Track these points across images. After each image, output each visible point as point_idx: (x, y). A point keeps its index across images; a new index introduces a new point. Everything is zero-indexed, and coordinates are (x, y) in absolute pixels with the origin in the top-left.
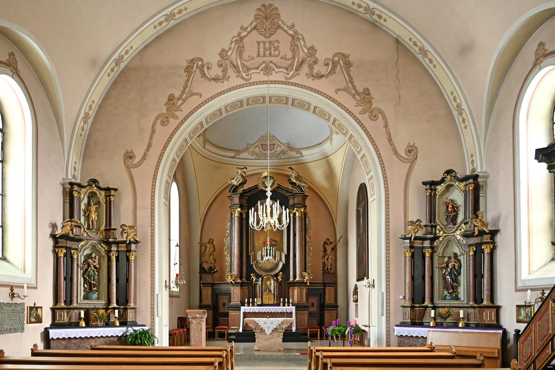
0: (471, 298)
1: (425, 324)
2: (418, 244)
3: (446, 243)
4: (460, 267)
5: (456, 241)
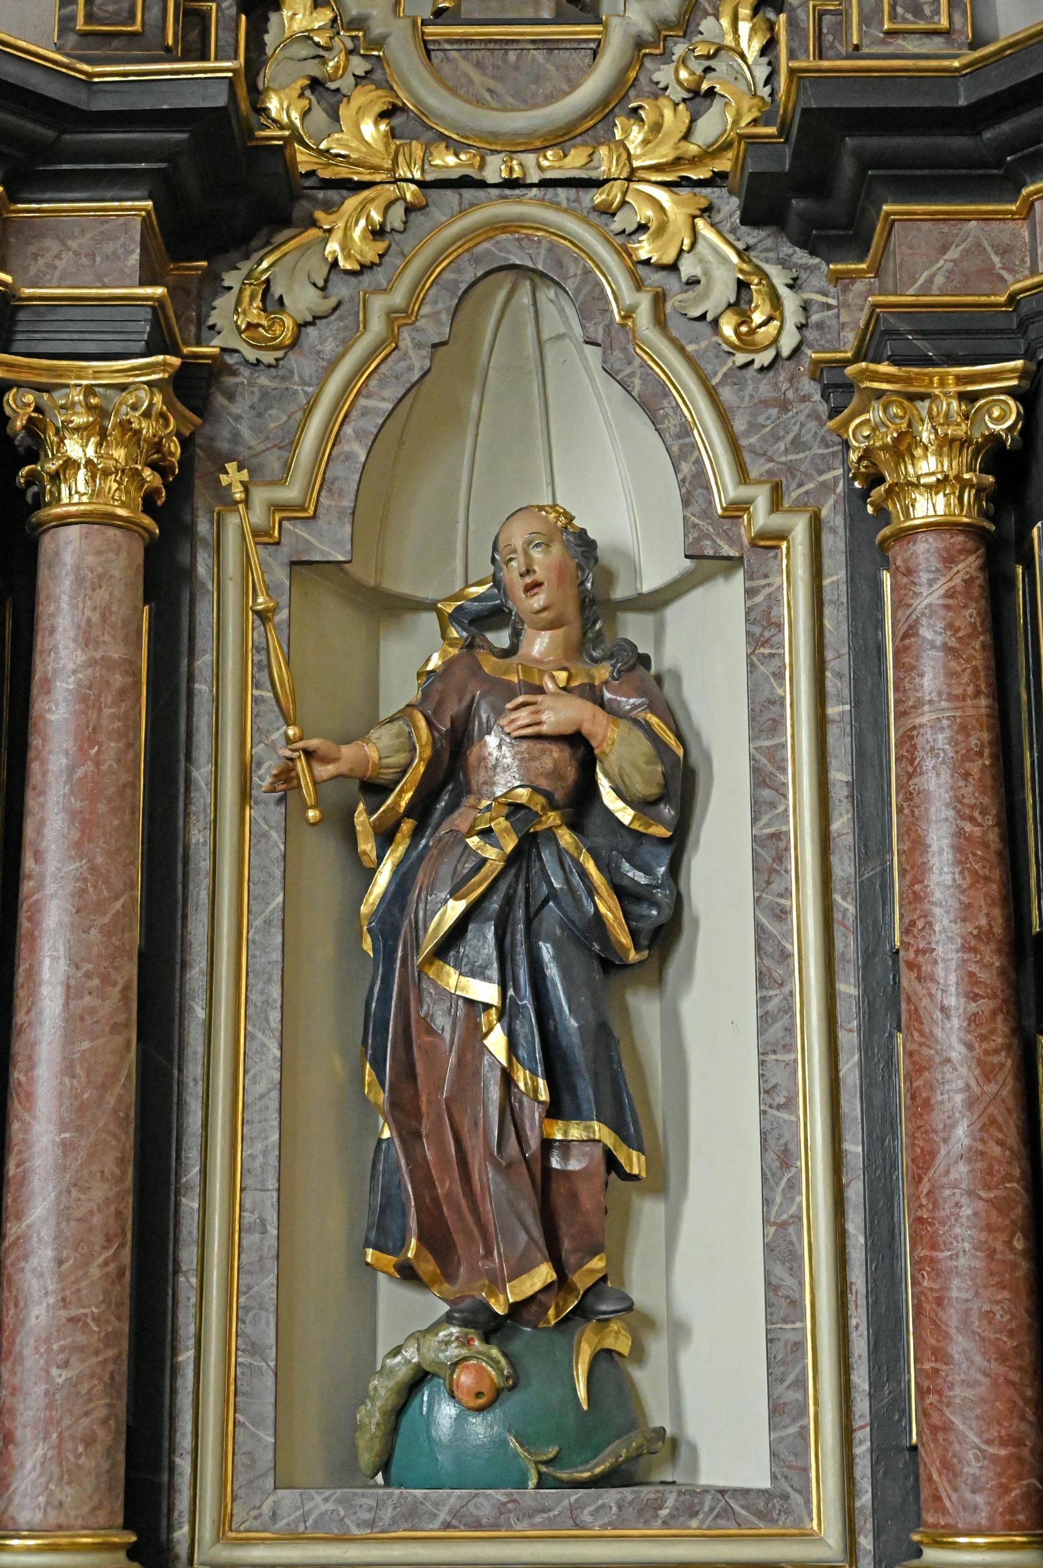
4: (679, 788)
5: (617, 286)
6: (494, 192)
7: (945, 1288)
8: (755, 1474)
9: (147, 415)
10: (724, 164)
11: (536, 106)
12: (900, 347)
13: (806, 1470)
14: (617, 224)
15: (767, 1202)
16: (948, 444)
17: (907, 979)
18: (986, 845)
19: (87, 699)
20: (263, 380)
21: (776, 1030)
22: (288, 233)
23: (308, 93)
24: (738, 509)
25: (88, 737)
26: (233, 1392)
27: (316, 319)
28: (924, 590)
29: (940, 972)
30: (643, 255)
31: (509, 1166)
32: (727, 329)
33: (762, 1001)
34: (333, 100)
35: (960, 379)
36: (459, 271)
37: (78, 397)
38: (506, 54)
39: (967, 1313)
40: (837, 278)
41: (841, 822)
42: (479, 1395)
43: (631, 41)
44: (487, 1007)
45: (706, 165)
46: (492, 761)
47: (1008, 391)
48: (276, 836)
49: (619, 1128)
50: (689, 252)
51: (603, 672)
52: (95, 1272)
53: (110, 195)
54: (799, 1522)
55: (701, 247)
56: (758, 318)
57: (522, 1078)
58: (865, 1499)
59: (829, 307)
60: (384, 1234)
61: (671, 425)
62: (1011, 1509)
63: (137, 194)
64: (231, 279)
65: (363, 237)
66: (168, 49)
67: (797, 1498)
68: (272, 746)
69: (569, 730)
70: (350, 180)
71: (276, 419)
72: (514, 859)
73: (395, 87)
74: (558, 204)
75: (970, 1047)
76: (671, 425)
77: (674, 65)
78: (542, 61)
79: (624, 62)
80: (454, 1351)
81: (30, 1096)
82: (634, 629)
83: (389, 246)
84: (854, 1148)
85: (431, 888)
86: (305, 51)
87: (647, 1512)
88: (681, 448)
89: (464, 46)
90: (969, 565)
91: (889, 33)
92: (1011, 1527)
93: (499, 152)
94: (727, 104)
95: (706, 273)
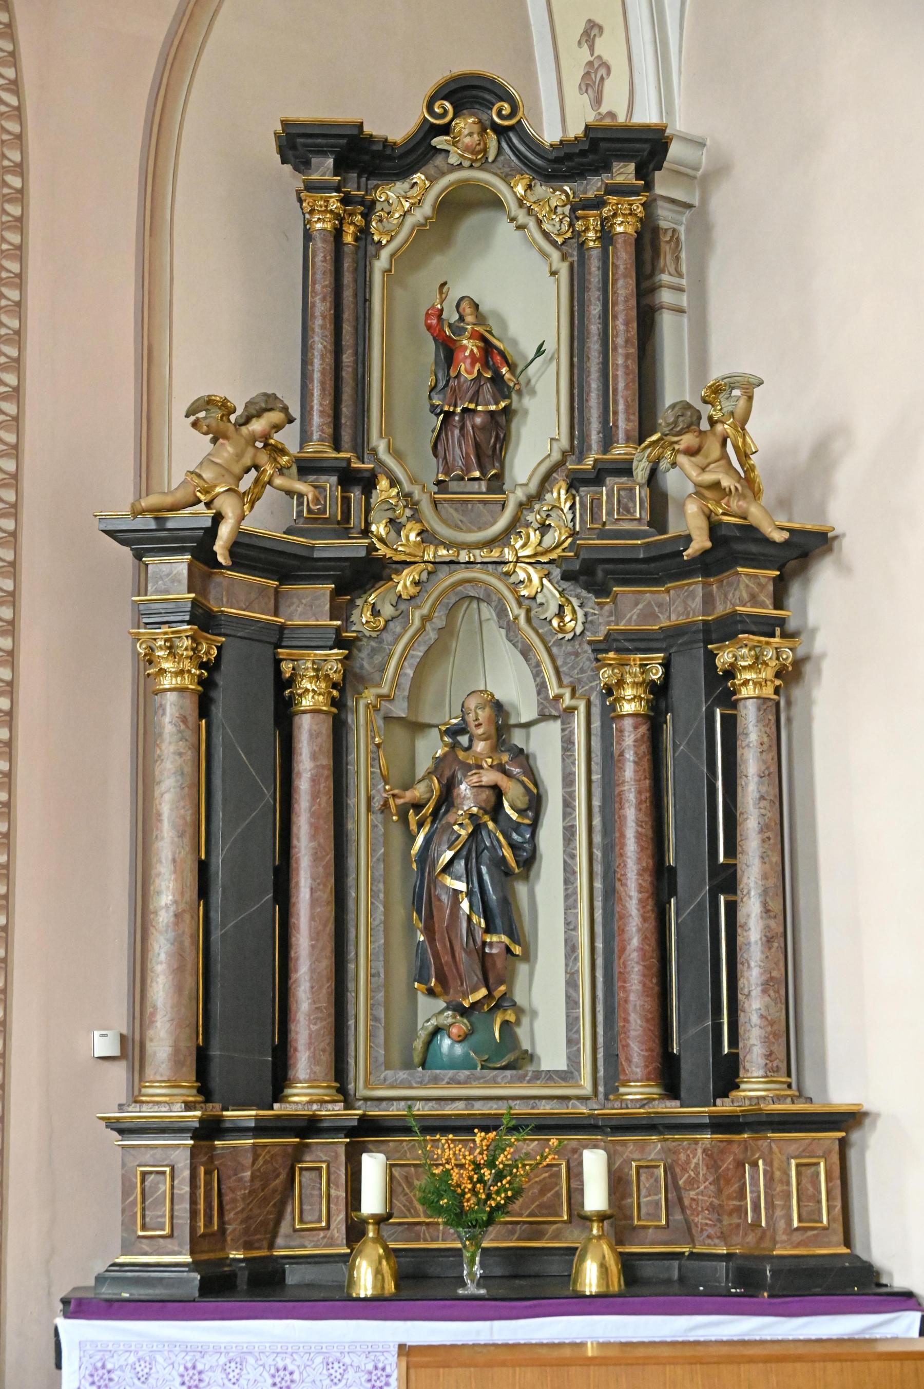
0: (637, 1051)
1: (294, 1276)
2: (240, 597)
3: (439, 620)
4: (535, 804)
5: (514, 610)
6: (463, 566)
7: (628, 997)
8: (561, 1064)
9: (335, 672)
12: (620, 645)
13: (580, 1063)
14: (513, 579)
15: (567, 965)
16: (635, 684)
17: (618, 884)
18: (646, 836)
19: (314, 781)
20: (373, 643)
21: (571, 900)
22: (382, 583)
24: (558, 697)
25: (315, 796)
26: (371, 1035)
27: (393, 618)
28: (627, 739)
29: (629, 882)
30: (522, 594)
31: (470, 952)
32: (555, 623)
33: (566, 890)
35: (641, 659)
36: (449, 599)
37: (309, 665)
39: (635, 1005)
40: (599, 604)
41: (597, 821)
42: (459, 1036)
44: (462, 892)
46: (462, 795)
47: (659, 664)
48: (380, 826)
49: (512, 935)
51: (505, 758)
52: (324, 991)
54: (577, 1081)
55: (545, 590)
56: (567, 619)
57: (475, 919)
58: (601, 1073)
59: (595, 614)
60: (422, 977)
61: (533, 662)
62: (649, 1073)
64: (359, 602)
67: (577, 1073)
68: (378, 791)
69: (492, 783)
71: (378, 659)
72: (471, 835)
75: (638, 910)
76: (533, 662)
80: (450, 1020)
81: (298, 928)
82: (517, 738)
84: (599, 945)
85: (440, 845)
87: (521, 1079)
88: (537, 672)
90: (643, 729)
92: (648, 1079)
95: (547, 601)
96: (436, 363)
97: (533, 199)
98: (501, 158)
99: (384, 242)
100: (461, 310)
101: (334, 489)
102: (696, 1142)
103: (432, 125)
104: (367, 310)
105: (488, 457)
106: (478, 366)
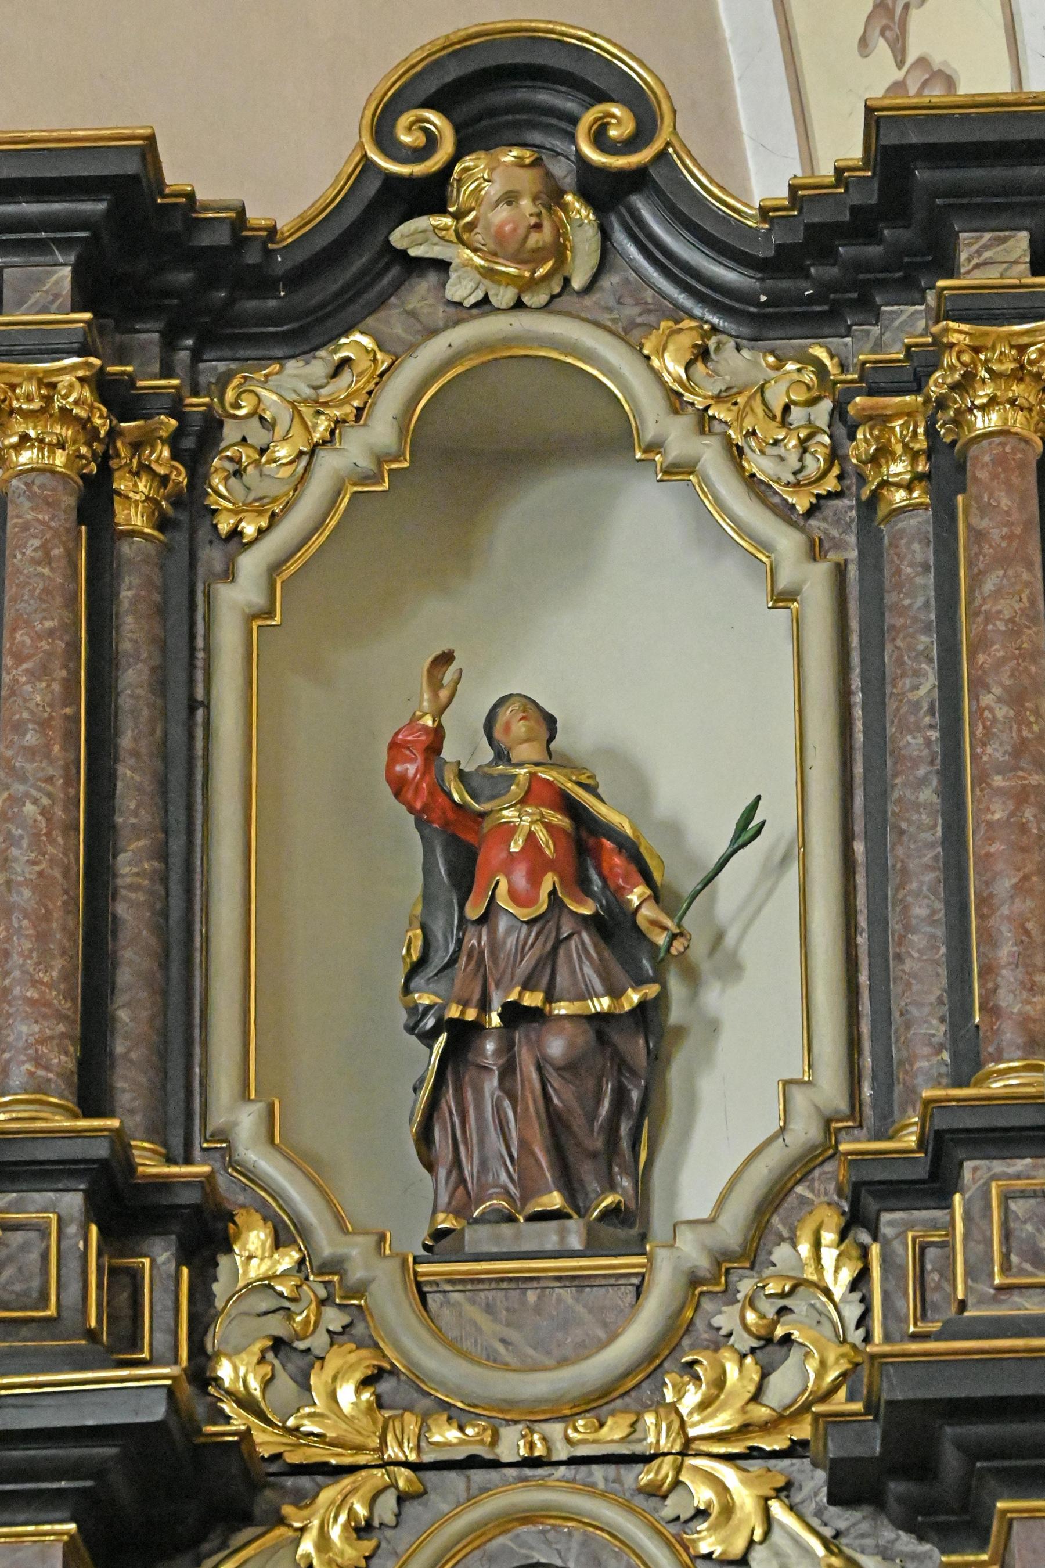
6: (512, 1472)
10: (803, 1431)
11: (563, 1362)
14: (672, 1507)
22: (248, 1533)
23: (270, 1356)
30: (704, 1548)
34: (302, 1362)
38: (524, 1294)
43: (684, 1280)
45: (782, 1432)
50: (762, 1542)
53: (22, 1517)
55: (777, 1536)
63: (57, 1515)
65: (346, 1539)
66: (92, 1335)
70: (326, 1464)
73: (382, 1344)
74: (593, 1485)
77: (740, 1305)
78: (570, 1301)
79: (675, 1305)
83: (378, 1546)
86: (265, 1303)
89: (469, 1287)
91: (1000, 1289)
93: (516, 1422)
94: (808, 1354)
96: (427, 898)
97: (715, 387)
98: (610, 281)
99: (249, 530)
100: (498, 733)
101: (72, 1229)
102: (868, 332)
103: (391, 179)
104: (199, 733)
105: (594, 1155)
106: (549, 882)
